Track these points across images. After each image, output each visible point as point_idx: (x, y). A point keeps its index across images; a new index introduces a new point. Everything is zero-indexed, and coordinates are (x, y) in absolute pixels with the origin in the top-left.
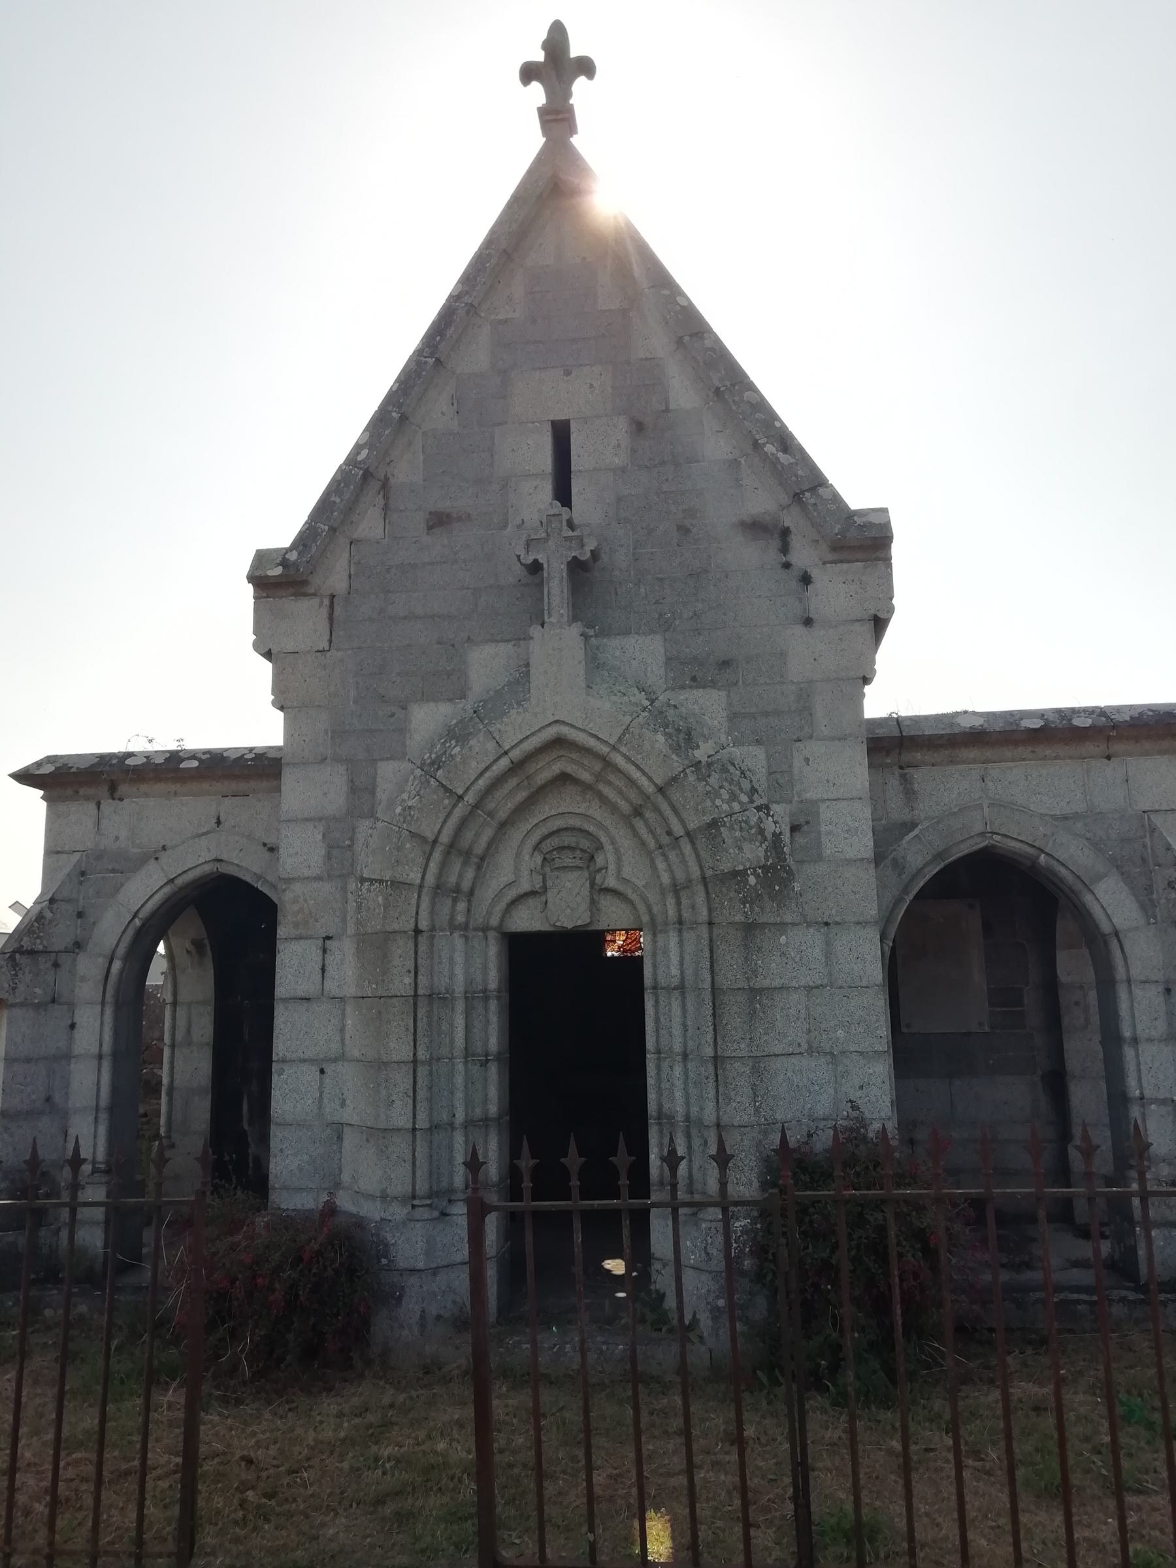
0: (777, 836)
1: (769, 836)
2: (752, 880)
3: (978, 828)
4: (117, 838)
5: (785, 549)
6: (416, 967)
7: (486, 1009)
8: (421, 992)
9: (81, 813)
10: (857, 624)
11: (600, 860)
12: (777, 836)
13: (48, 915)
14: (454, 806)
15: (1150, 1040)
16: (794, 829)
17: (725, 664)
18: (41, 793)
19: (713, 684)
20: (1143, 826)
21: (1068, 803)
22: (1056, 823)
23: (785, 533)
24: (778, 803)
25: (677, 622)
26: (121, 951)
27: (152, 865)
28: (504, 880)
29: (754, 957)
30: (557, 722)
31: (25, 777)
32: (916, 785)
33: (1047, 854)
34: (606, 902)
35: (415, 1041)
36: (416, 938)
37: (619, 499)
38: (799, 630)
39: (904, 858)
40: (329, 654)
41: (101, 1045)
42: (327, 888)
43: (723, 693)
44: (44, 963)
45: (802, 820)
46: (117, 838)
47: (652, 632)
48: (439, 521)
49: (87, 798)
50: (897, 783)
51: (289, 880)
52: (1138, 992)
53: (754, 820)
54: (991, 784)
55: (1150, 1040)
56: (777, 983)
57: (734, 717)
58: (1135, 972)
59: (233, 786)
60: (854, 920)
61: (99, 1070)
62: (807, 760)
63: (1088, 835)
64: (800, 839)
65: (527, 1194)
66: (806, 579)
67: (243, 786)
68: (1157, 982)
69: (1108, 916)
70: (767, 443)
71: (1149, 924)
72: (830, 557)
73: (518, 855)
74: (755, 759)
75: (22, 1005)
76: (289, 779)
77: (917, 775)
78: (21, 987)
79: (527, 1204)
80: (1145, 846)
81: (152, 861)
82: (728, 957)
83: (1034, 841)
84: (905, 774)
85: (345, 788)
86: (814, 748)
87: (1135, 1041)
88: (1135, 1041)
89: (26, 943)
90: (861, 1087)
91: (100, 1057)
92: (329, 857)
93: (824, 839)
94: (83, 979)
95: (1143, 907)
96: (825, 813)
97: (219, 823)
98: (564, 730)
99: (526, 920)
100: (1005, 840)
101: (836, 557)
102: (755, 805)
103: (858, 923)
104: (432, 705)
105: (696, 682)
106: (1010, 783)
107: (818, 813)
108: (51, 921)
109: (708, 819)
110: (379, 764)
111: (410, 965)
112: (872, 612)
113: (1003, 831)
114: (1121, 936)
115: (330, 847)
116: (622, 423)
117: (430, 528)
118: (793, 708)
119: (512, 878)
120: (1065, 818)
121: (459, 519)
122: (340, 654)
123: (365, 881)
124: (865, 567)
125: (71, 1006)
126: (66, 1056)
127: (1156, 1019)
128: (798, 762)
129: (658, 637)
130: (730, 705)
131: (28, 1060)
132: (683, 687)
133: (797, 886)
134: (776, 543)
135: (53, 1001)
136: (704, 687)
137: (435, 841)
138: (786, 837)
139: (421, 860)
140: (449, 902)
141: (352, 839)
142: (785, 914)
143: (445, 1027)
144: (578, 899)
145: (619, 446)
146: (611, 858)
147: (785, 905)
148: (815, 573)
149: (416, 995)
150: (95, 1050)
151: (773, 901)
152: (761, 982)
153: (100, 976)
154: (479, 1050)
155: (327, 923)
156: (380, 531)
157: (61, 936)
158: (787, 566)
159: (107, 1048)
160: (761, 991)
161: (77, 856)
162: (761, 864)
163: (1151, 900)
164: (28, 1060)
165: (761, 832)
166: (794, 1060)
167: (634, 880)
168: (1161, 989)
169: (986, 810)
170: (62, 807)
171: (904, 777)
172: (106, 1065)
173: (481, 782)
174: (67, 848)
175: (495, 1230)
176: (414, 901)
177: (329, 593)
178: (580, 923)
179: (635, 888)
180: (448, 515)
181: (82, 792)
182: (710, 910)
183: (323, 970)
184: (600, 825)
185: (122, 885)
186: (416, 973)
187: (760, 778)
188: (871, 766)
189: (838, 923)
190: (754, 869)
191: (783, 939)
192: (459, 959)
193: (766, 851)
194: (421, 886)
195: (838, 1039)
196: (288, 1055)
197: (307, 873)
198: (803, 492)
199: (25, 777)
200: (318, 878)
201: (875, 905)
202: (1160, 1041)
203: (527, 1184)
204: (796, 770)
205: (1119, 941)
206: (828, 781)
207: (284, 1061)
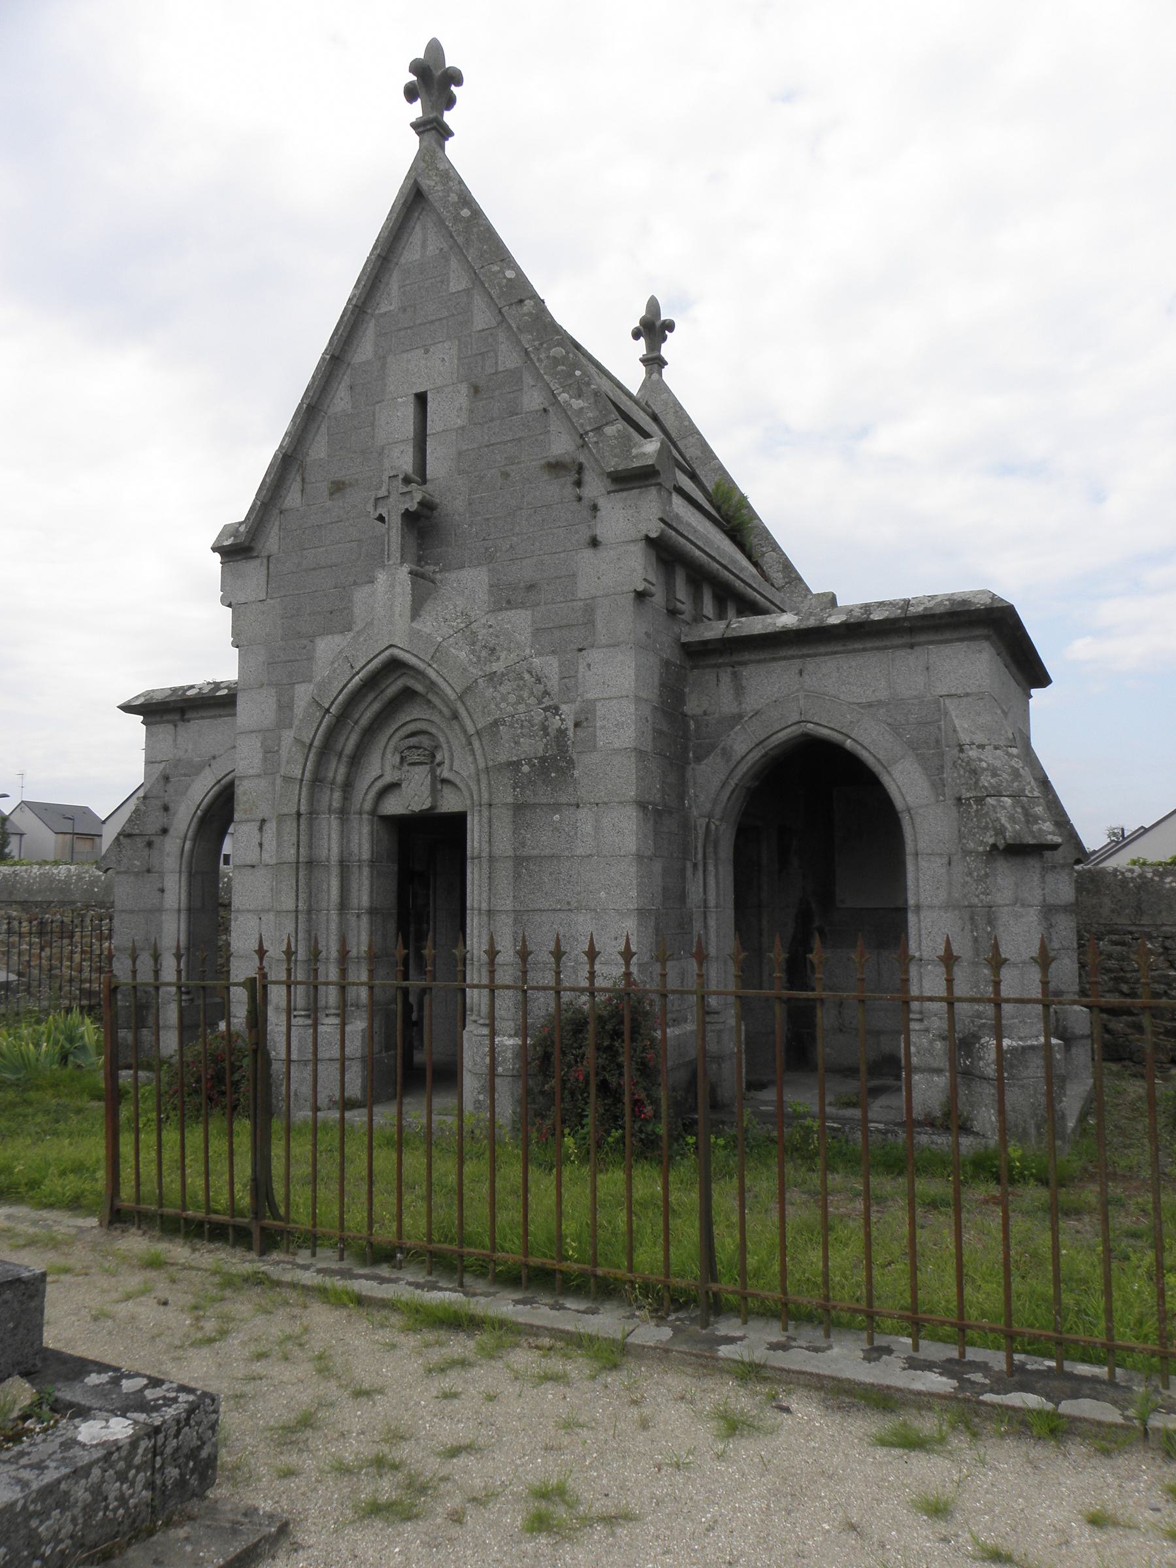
0: (562, 732)
1: (552, 731)
2: (526, 769)
3: (795, 717)
4: (186, 751)
5: (579, 483)
6: (298, 842)
7: (360, 873)
8: (301, 860)
9: (165, 731)
10: (632, 544)
11: (438, 758)
12: (562, 732)
13: (143, 808)
14: (324, 717)
15: (931, 907)
16: (577, 725)
17: (531, 587)
18: (141, 718)
19: (523, 605)
20: (939, 710)
21: (874, 691)
22: (862, 711)
23: (580, 468)
24: (565, 703)
25: (498, 555)
26: (190, 834)
27: (207, 770)
28: (375, 774)
29: (523, 831)
30: (391, 646)
31: (127, 708)
32: (744, 681)
33: (854, 740)
34: (447, 791)
35: (297, 896)
36: (298, 820)
37: (460, 454)
38: (588, 553)
39: (731, 747)
40: (265, 603)
41: (180, 903)
42: (263, 783)
43: (529, 612)
44: (140, 843)
45: (583, 717)
47: (480, 564)
48: (338, 488)
49: (168, 722)
50: (729, 680)
52: (923, 864)
53: (538, 719)
54: (807, 677)
55: (931, 907)
56: (547, 852)
57: (537, 632)
58: (922, 845)
60: (617, 800)
61: (179, 920)
62: (589, 665)
63: (889, 720)
64: (581, 734)
66: (595, 508)
68: (941, 854)
69: (902, 795)
70: (563, 392)
71: (937, 801)
72: (613, 488)
73: (384, 754)
74: (550, 667)
75: (125, 872)
76: (243, 704)
77: (745, 672)
78: (125, 860)
80: (939, 729)
81: (207, 767)
82: (501, 832)
83: (842, 728)
84: (735, 672)
85: (275, 706)
86: (594, 655)
87: (918, 908)
88: (918, 908)
89: (128, 831)
90: (616, 939)
91: (179, 911)
92: (265, 759)
93: (598, 733)
95: (933, 785)
96: (600, 710)
98: (396, 651)
99: (394, 806)
100: (818, 728)
101: (617, 487)
102: (543, 706)
103: (621, 803)
104: (330, 637)
105: (510, 604)
106: (823, 675)
107: (595, 710)
108: (145, 813)
109: (490, 719)
110: (296, 686)
111: (294, 839)
112: (644, 532)
113: (816, 719)
114: (912, 812)
115: (266, 752)
116: (464, 389)
117: (331, 494)
118: (581, 622)
119: (379, 772)
120: (870, 705)
121: (351, 485)
122: (272, 602)
124: (640, 493)
125: (161, 875)
126: (160, 910)
127: (938, 888)
128: (582, 668)
129: (485, 569)
130: (534, 622)
131: (132, 912)
132: (500, 610)
133: (576, 773)
135: (149, 871)
136: (516, 608)
137: (311, 745)
138: (571, 733)
139: (302, 760)
140: (328, 792)
141: (279, 745)
142: (560, 796)
143: (325, 887)
144: (423, 788)
145: (461, 408)
146: (447, 755)
147: (560, 789)
148: (601, 503)
149: (298, 862)
150: (176, 906)
151: (547, 786)
152: (526, 852)
153: (179, 853)
154: (356, 906)
155: (264, 810)
156: (299, 501)
157: (152, 825)
158: (580, 499)
159: (183, 905)
160: (528, 859)
161: (162, 766)
162: (539, 755)
163: (942, 779)
164: (132, 912)
165: (545, 728)
166: (561, 915)
167: (461, 772)
168: (945, 860)
169: (802, 702)
170: (154, 729)
171: (734, 674)
172: (183, 916)
173: (340, 697)
175: (360, 1039)
176: (297, 792)
177: (266, 554)
178: (424, 807)
179: (463, 779)
180: (343, 483)
181: (165, 718)
182: (490, 794)
183: (261, 845)
184: (439, 728)
186: (298, 846)
187: (554, 684)
189: (605, 803)
190: (530, 760)
191: (557, 817)
192: (335, 836)
193: (546, 745)
194: (302, 780)
195: (600, 898)
196: (241, 907)
197: (251, 772)
198: (587, 433)
199: (127, 708)
200: (259, 776)
201: (634, 788)
202: (940, 908)
204: (580, 676)
205: (911, 818)
206: (604, 683)
207: (238, 911)
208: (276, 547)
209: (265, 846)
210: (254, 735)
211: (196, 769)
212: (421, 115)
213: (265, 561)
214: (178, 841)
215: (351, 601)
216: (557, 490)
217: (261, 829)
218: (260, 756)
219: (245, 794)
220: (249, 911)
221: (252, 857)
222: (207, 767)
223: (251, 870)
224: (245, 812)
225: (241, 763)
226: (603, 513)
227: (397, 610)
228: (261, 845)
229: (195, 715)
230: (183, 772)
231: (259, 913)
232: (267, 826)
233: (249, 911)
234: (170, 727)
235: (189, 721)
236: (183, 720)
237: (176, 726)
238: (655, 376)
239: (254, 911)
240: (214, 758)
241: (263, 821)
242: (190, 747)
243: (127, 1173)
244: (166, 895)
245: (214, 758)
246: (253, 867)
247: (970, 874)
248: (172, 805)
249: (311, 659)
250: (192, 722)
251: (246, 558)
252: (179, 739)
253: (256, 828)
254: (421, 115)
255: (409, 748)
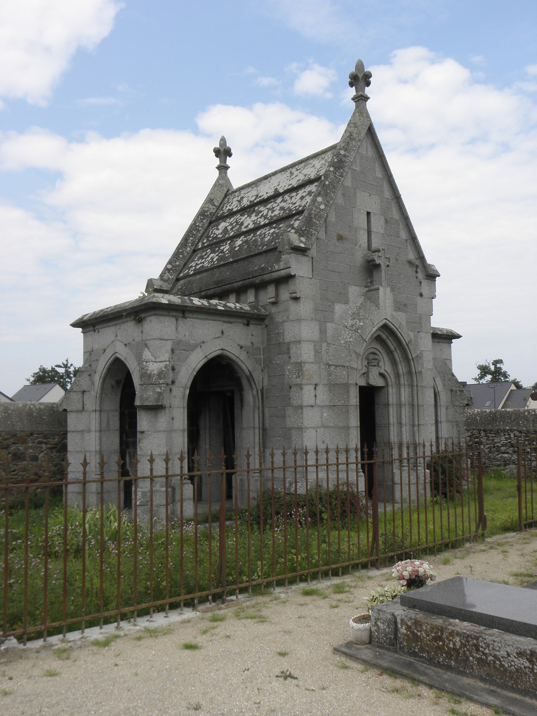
4: (185, 336)
17: (405, 305)
19: (403, 311)
27: (198, 349)
38: (419, 298)
46: (185, 336)
49: (173, 316)
51: (305, 363)
59: (228, 319)
65: (366, 459)
66: (421, 282)
67: (232, 320)
79: (366, 462)
81: (199, 347)
85: (319, 331)
94: (175, 397)
97: (222, 333)
110: (327, 323)
117: (338, 240)
122: (315, 280)
123: (489, 374)
134: (415, 269)
155: (316, 380)
158: (417, 278)
174: (165, 338)
183: (316, 396)
185: (188, 356)
188: (432, 342)
197: (309, 360)
200: (313, 363)
203: (366, 456)
208: (316, 254)
209: (318, 397)
210: (309, 342)
211: (193, 348)
212: (355, 94)
213: (311, 259)
214: (181, 389)
215: (347, 291)
216: (410, 271)
217: (315, 389)
218: (313, 353)
219: (307, 371)
220: (311, 428)
221: (311, 402)
222: (199, 347)
223: (311, 408)
224: (307, 380)
225: (304, 356)
226: (422, 285)
227: (387, 304)
228: (316, 396)
229: (191, 316)
230: (183, 348)
231: (316, 428)
232: (318, 388)
233: (311, 428)
234: (173, 320)
235: (186, 318)
236: (183, 317)
237: (177, 320)
238: (223, 175)
239: (314, 428)
240: (203, 342)
241: (316, 385)
242: (187, 334)
243: (524, 511)
244: (174, 422)
245: (203, 342)
246: (312, 406)
247: (457, 412)
248: (176, 367)
249: (333, 312)
250: (188, 319)
251: (303, 255)
252: (180, 328)
253: (313, 388)
254: (355, 94)
255: (374, 359)
